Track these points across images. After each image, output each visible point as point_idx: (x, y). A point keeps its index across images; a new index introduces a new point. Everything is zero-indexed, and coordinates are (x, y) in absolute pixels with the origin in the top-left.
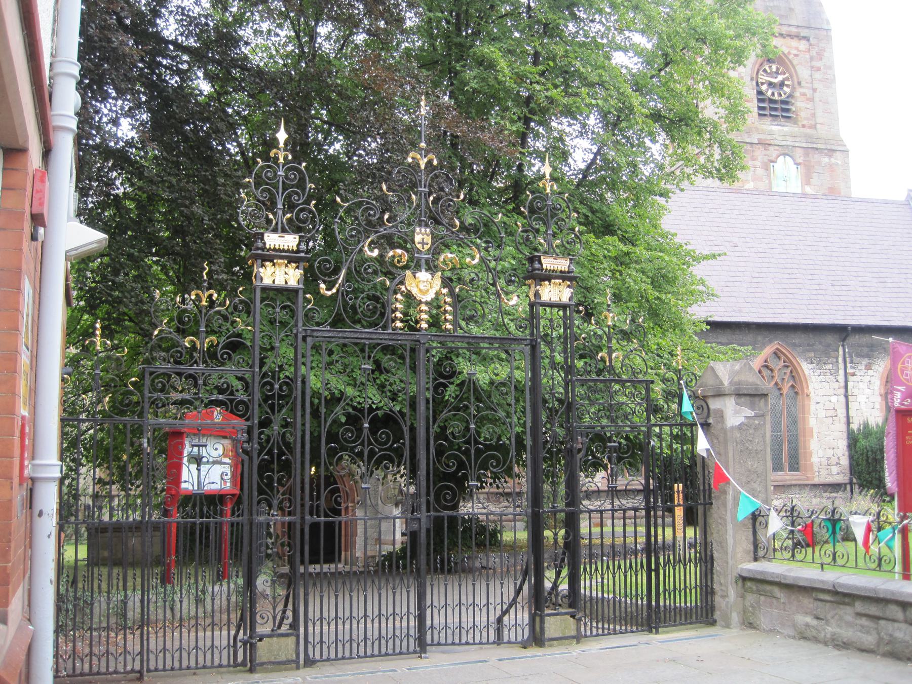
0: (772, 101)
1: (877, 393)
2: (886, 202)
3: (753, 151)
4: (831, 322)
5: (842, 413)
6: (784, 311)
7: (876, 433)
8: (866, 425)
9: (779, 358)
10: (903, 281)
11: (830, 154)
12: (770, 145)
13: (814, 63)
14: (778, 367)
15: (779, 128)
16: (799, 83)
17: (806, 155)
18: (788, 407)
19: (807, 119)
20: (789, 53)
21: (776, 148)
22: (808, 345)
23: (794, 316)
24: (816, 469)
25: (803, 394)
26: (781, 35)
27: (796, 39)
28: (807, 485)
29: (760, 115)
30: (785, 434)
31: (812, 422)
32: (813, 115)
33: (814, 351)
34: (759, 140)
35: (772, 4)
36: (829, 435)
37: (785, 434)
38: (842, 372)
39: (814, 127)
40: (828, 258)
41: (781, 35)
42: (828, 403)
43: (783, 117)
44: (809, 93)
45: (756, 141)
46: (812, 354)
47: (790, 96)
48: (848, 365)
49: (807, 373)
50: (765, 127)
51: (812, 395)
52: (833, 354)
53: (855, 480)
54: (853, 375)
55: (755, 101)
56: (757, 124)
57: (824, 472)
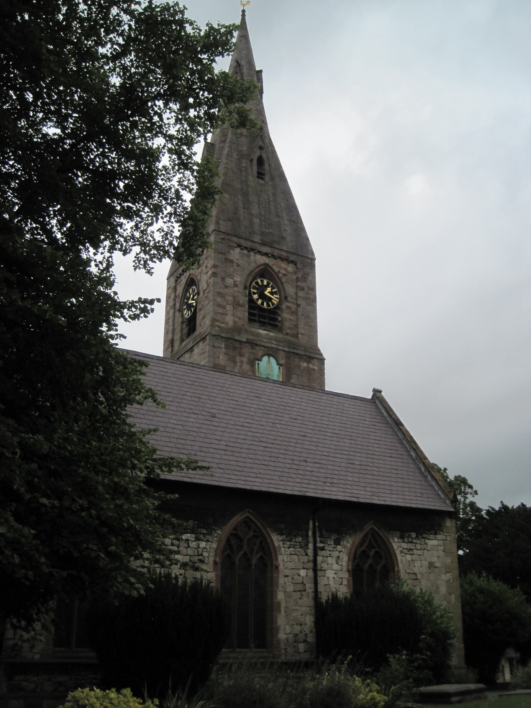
0: (261, 309)
1: (345, 569)
3: (241, 348)
5: (310, 587)
6: (256, 480)
12: (257, 345)
13: (300, 284)
16: (286, 298)
19: (290, 328)
20: (279, 272)
21: (262, 348)
24: (283, 646)
26: (273, 256)
27: (285, 261)
29: (250, 320)
31: (280, 596)
32: (296, 326)
34: (247, 339)
35: (267, 231)
36: (297, 610)
38: (311, 546)
39: (296, 336)
42: (296, 577)
44: (293, 307)
46: (283, 526)
48: (318, 539)
49: (276, 544)
50: (253, 330)
51: (281, 567)
54: (323, 549)
56: (246, 326)
57: (290, 650)
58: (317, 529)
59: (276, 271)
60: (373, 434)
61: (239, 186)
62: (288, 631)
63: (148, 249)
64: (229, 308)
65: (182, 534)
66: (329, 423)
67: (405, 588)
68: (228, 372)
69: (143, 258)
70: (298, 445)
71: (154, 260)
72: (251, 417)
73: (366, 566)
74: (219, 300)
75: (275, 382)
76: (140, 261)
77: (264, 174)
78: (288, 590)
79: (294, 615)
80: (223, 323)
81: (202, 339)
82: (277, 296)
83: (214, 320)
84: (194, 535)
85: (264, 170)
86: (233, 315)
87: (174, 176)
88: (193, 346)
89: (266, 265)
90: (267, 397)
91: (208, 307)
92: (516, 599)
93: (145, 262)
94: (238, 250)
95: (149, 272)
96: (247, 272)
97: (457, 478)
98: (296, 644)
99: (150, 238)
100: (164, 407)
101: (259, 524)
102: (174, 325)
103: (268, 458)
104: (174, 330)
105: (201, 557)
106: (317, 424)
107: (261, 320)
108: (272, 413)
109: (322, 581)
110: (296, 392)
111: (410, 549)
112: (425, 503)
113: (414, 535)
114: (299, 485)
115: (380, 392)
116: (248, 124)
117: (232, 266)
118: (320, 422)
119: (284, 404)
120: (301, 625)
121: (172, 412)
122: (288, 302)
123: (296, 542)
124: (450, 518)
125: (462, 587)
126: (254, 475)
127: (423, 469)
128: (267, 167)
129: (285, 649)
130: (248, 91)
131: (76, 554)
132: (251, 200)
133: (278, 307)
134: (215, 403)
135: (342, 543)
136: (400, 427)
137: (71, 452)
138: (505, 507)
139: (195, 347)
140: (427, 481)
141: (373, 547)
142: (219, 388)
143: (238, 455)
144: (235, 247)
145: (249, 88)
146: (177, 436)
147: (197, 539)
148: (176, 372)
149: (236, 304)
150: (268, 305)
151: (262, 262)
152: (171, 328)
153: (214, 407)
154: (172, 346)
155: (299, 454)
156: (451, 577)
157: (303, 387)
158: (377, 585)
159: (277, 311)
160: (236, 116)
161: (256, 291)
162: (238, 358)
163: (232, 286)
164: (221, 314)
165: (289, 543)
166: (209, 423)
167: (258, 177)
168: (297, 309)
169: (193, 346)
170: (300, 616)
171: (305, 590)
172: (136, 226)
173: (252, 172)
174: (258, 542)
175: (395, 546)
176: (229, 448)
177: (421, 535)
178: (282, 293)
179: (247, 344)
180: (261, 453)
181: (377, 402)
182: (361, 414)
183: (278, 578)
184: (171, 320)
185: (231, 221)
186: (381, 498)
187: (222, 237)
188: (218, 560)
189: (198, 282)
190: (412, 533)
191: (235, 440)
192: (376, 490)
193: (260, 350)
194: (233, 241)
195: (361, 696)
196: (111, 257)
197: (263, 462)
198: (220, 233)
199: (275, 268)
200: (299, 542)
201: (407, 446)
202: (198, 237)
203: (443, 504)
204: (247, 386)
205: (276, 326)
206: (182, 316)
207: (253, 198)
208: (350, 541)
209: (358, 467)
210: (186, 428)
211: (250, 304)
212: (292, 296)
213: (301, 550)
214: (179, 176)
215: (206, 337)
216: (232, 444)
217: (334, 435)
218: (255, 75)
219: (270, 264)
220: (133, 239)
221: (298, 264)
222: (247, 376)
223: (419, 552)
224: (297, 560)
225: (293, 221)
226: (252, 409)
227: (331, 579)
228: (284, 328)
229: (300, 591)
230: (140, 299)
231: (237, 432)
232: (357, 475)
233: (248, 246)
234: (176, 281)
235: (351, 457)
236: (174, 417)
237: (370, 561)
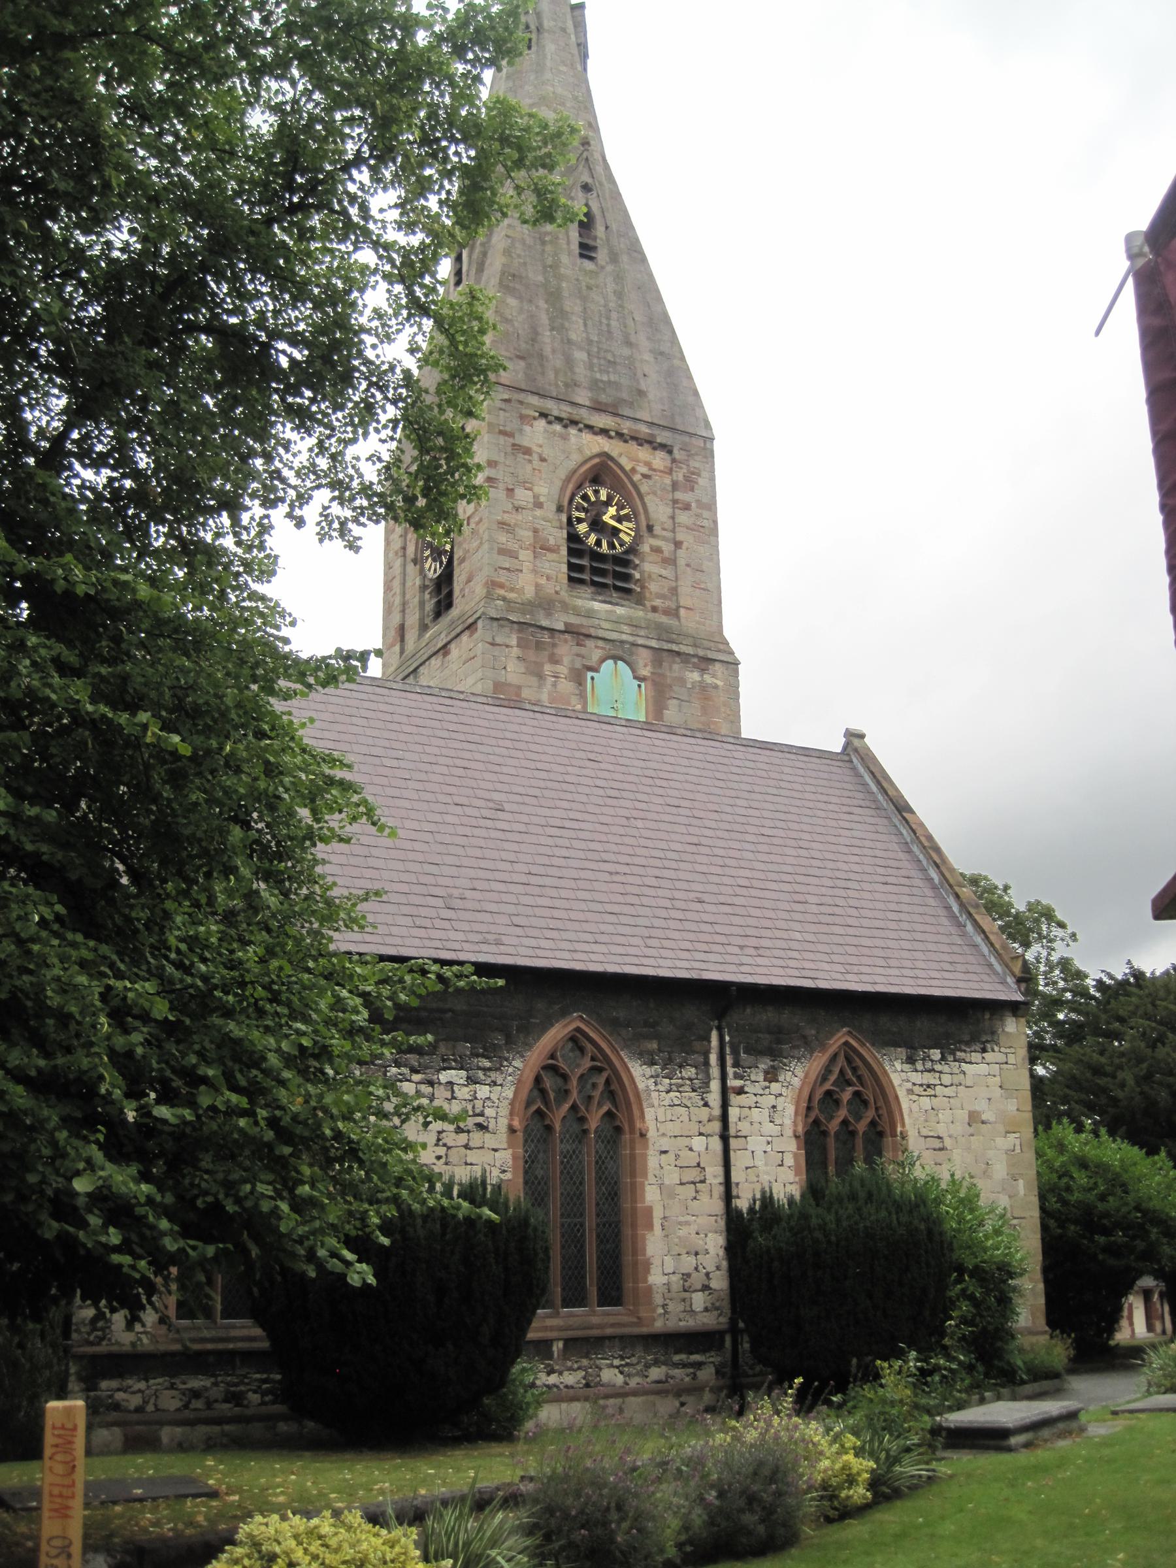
0: (597, 556)
1: (789, 1132)
3: (554, 645)
4: (694, 975)
5: (715, 1173)
6: (595, 947)
7: (791, 1216)
8: (767, 1200)
9: (582, 1050)
10: (841, 902)
11: (703, 666)
12: (588, 636)
13: (679, 495)
15: (608, 607)
16: (650, 528)
17: (657, 662)
18: (600, 1163)
20: (633, 470)
21: (600, 643)
23: (619, 959)
24: (658, 1300)
25: (632, 1131)
26: (620, 435)
27: (646, 446)
29: (571, 579)
30: (590, 1221)
31: (651, 1195)
32: (674, 591)
33: (657, 1037)
34: (566, 624)
35: (605, 378)
36: (687, 1223)
37: (590, 1221)
38: (715, 1085)
39: (674, 613)
40: (693, 849)
41: (620, 435)
42: (685, 1153)
44: (668, 548)
45: (561, 627)
47: (632, 550)
48: (730, 1071)
49: (641, 1086)
50: (579, 602)
51: (652, 1133)
52: (697, 1045)
53: (741, 1325)
54: (740, 1091)
58: (728, 1050)
59: (628, 468)
60: (847, 833)
61: (540, 278)
62: (669, 1269)
63: (347, 494)
65: (438, 1071)
66: (751, 812)
67: (918, 1173)
68: (528, 706)
69: (338, 518)
70: (682, 865)
71: (362, 520)
72: (580, 806)
73: (834, 1126)
74: (502, 538)
75: (629, 724)
76: (332, 522)
77: (594, 249)
78: (667, 1182)
80: (512, 590)
81: (468, 628)
82: (631, 525)
83: (492, 585)
84: (463, 1073)
85: (595, 238)
86: (535, 571)
87: (399, 331)
88: (449, 642)
89: (606, 455)
90: (612, 759)
91: (480, 554)
92: (1157, 1178)
93: (343, 524)
94: (541, 424)
95: (353, 546)
96: (562, 473)
97: (1031, 907)
98: (687, 1295)
99: (351, 471)
100: (393, 834)
101: (603, 1045)
102: (404, 594)
103: (620, 899)
104: (404, 604)
105: (480, 1120)
106: (724, 817)
107: (596, 579)
108: (625, 794)
109: (738, 1161)
110: (675, 746)
111: (929, 1086)
112: (960, 984)
113: (936, 1054)
114: (686, 955)
115: (862, 736)
116: (559, 215)
117: (530, 461)
118: (728, 809)
119: (652, 773)
120: (697, 1254)
121: (407, 804)
122: (654, 536)
124: (1015, 1015)
125: (1039, 1154)
126: (589, 938)
127: (956, 908)
128: (600, 231)
129: (664, 1306)
130: (557, 141)
131: (231, 1208)
132: (568, 309)
133: (632, 550)
134: (502, 778)
135: (781, 1078)
136: (905, 814)
137: (205, 979)
138: (1138, 975)
139: (453, 646)
140: (964, 935)
142: (508, 744)
143: (554, 893)
145: (559, 134)
146: (420, 857)
147: (472, 1081)
148: (415, 712)
149: (541, 547)
150: (612, 546)
151: (596, 450)
152: (398, 600)
153: (499, 786)
154: (402, 640)
155: (685, 886)
156: (1018, 1142)
157: (691, 732)
158: (860, 1167)
159: (631, 557)
160: (533, 198)
161: (583, 515)
162: (548, 668)
164: (508, 569)
166: (489, 823)
167: (582, 256)
169: (449, 642)
170: (694, 1235)
171: (703, 1181)
172: (320, 444)
173: (568, 243)
174: (601, 1080)
175: (896, 1079)
176: (533, 880)
177: (953, 1053)
178: (642, 517)
179: (567, 636)
180: (604, 887)
181: (855, 760)
182: (820, 790)
183: (645, 1157)
184: (396, 584)
186: (865, 978)
187: (506, 397)
188: (516, 1123)
191: (546, 861)
192: (853, 960)
194: (529, 406)
195: (825, 1463)
196: (267, 517)
197: (609, 908)
199: (623, 461)
200: (691, 1079)
201: (921, 857)
202: (457, 476)
203: (1000, 987)
204: (570, 736)
205: (628, 591)
206: (422, 572)
207: (572, 305)
208: (800, 1071)
209: (815, 909)
210: (439, 838)
211: (574, 561)
214: (409, 330)
215: (475, 622)
216: (541, 870)
217: (762, 839)
218: (569, 16)
219: (614, 454)
220: (315, 473)
221: (676, 451)
222: (569, 714)
223: (949, 1091)
224: (685, 1118)
225: (662, 353)
226: (581, 789)
227: (759, 1153)
229: (694, 1183)
230: (339, 650)
231: (550, 841)
232: (813, 928)
233: (564, 415)
235: (798, 888)
236: (413, 814)
237: (843, 1113)
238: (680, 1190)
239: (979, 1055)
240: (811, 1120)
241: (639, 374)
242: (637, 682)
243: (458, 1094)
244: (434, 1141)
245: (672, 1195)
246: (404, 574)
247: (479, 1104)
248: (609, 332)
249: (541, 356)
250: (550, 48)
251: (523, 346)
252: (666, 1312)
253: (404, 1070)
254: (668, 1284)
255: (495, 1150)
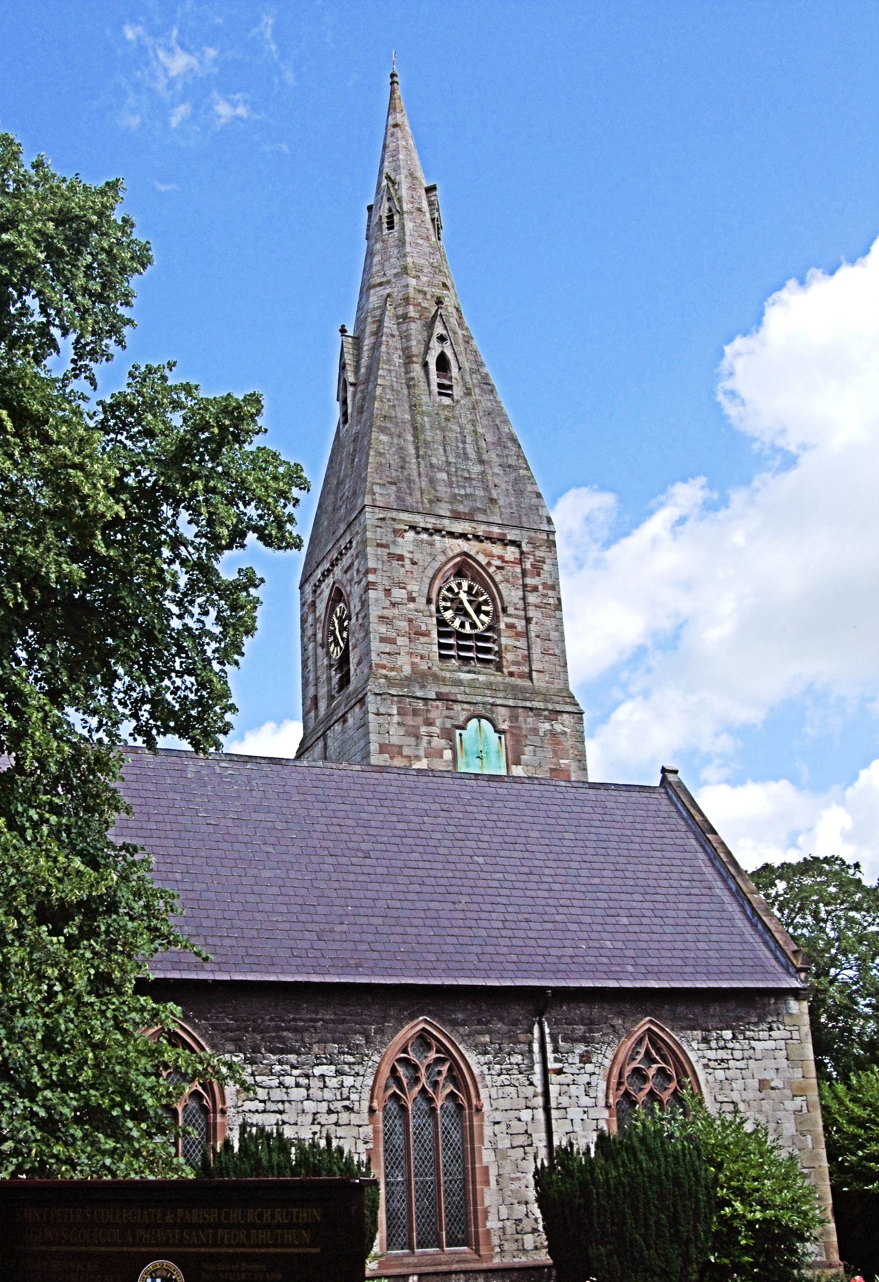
0: (461, 636)
2: (629, 788)
3: (428, 711)
11: (553, 717)
13: (529, 581)
14: (426, 1062)
16: (504, 610)
17: (514, 718)
21: (466, 706)
22: (480, 1022)
26: (477, 537)
28: (479, 1271)
31: (487, 1157)
32: (528, 659)
33: (490, 1032)
35: (462, 492)
36: (518, 1179)
38: (538, 1068)
41: (477, 537)
42: (515, 1123)
43: (480, 660)
48: (550, 1056)
49: (476, 1071)
51: (486, 1108)
55: (434, 634)
59: (484, 563)
61: (407, 417)
62: (504, 1215)
64: (401, 641)
65: (313, 1067)
78: (500, 1146)
79: (513, 1187)
80: (392, 669)
84: (333, 1068)
88: (346, 713)
89: (466, 554)
94: (411, 535)
98: (518, 1236)
102: (316, 671)
105: (347, 1103)
111: (722, 1060)
113: (728, 1034)
117: (403, 566)
122: (510, 616)
123: (511, 1064)
129: (500, 1246)
135: (594, 1060)
141: (655, 1061)
144: (406, 531)
147: (339, 1073)
151: (457, 551)
156: (804, 1104)
161: (449, 604)
163: (405, 601)
164: (389, 654)
165: (498, 1067)
168: (527, 626)
169: (346, 713)
170: (523, 1188)
171: (531, 1145)
174: (445, 1068)
175: (692, 1056)
179: (439, 703)
185: (395, 484)
187: (381, 516)
189: (348, 596)
190: (724, 1032)
193: (463, 710)
198: (377, 510)
200: (517, 1064)
206: (328, 654)
211: (443, 641)
212: (515, 604)
213: (520, 1076)
219: (472, 553)
221: (523, 545)
223: (741, 1064)
224: (514, 1095)
225: (509, 466)
228: (505, 663)
229: (523, 1147)
233: (429, 526)
234: (315, 592)
238: (511, 1152)
239: (766, 1033)
240: (621, 1092)
241: (491, 485)
242: (497, 735)
243: (328, 1083)
244: (310, 1120)
245: (505, 1157)
246: (316, 655)
247: (345, 1091)
248: (465, 454)
249: (409, 481)
250: (409, 226)
251: (394, 474)
252: (502, 1251)
253: (287, 1067)
254: (503, 1228)
255: (359, 1126)
